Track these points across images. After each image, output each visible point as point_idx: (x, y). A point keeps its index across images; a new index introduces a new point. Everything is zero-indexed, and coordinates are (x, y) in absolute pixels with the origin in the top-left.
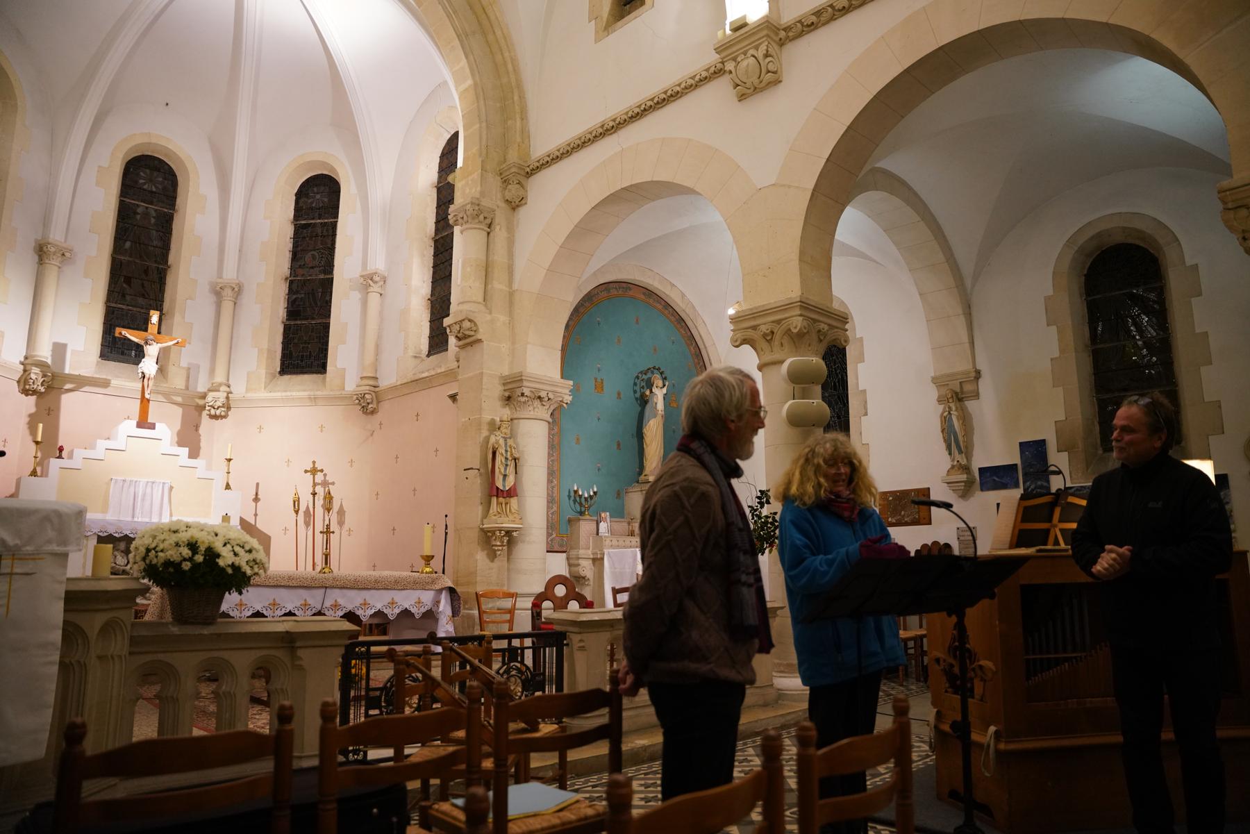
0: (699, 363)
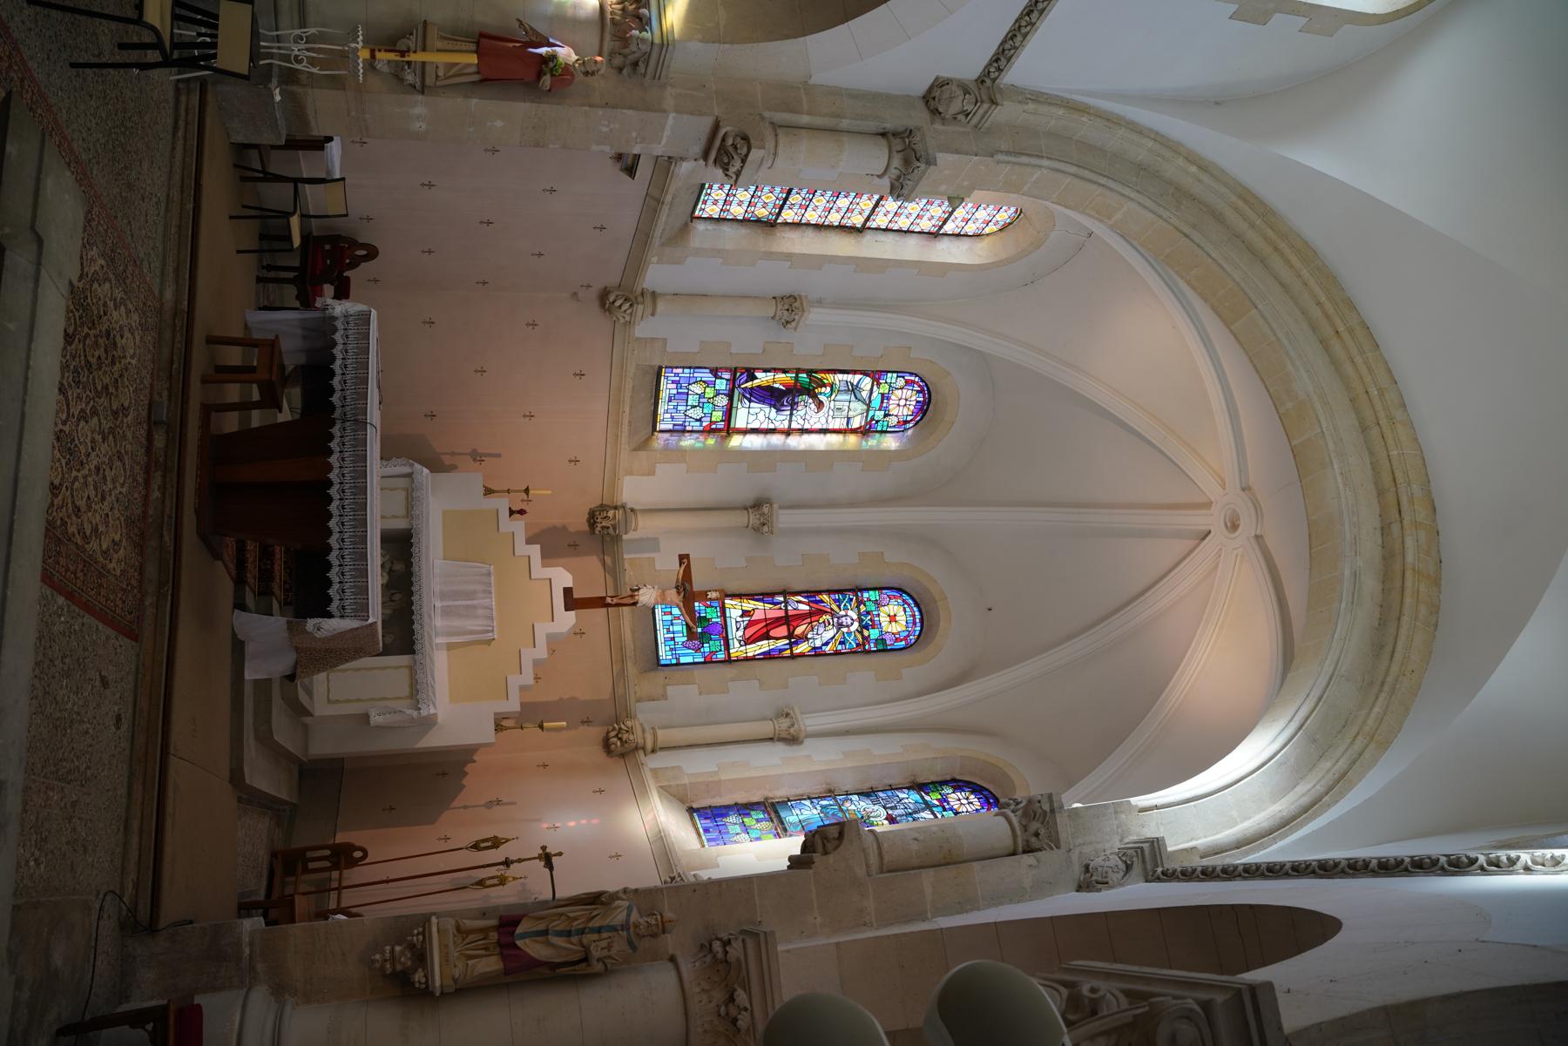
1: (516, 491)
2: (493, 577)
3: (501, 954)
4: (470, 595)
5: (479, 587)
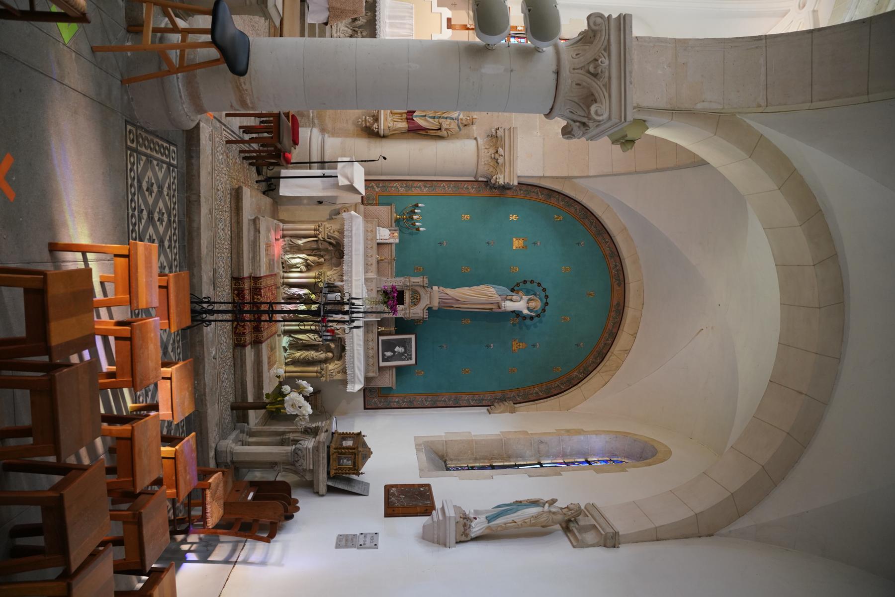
0: (562, 384)
3: (407, 122)
4: (402, 18)
5: (407, 14)
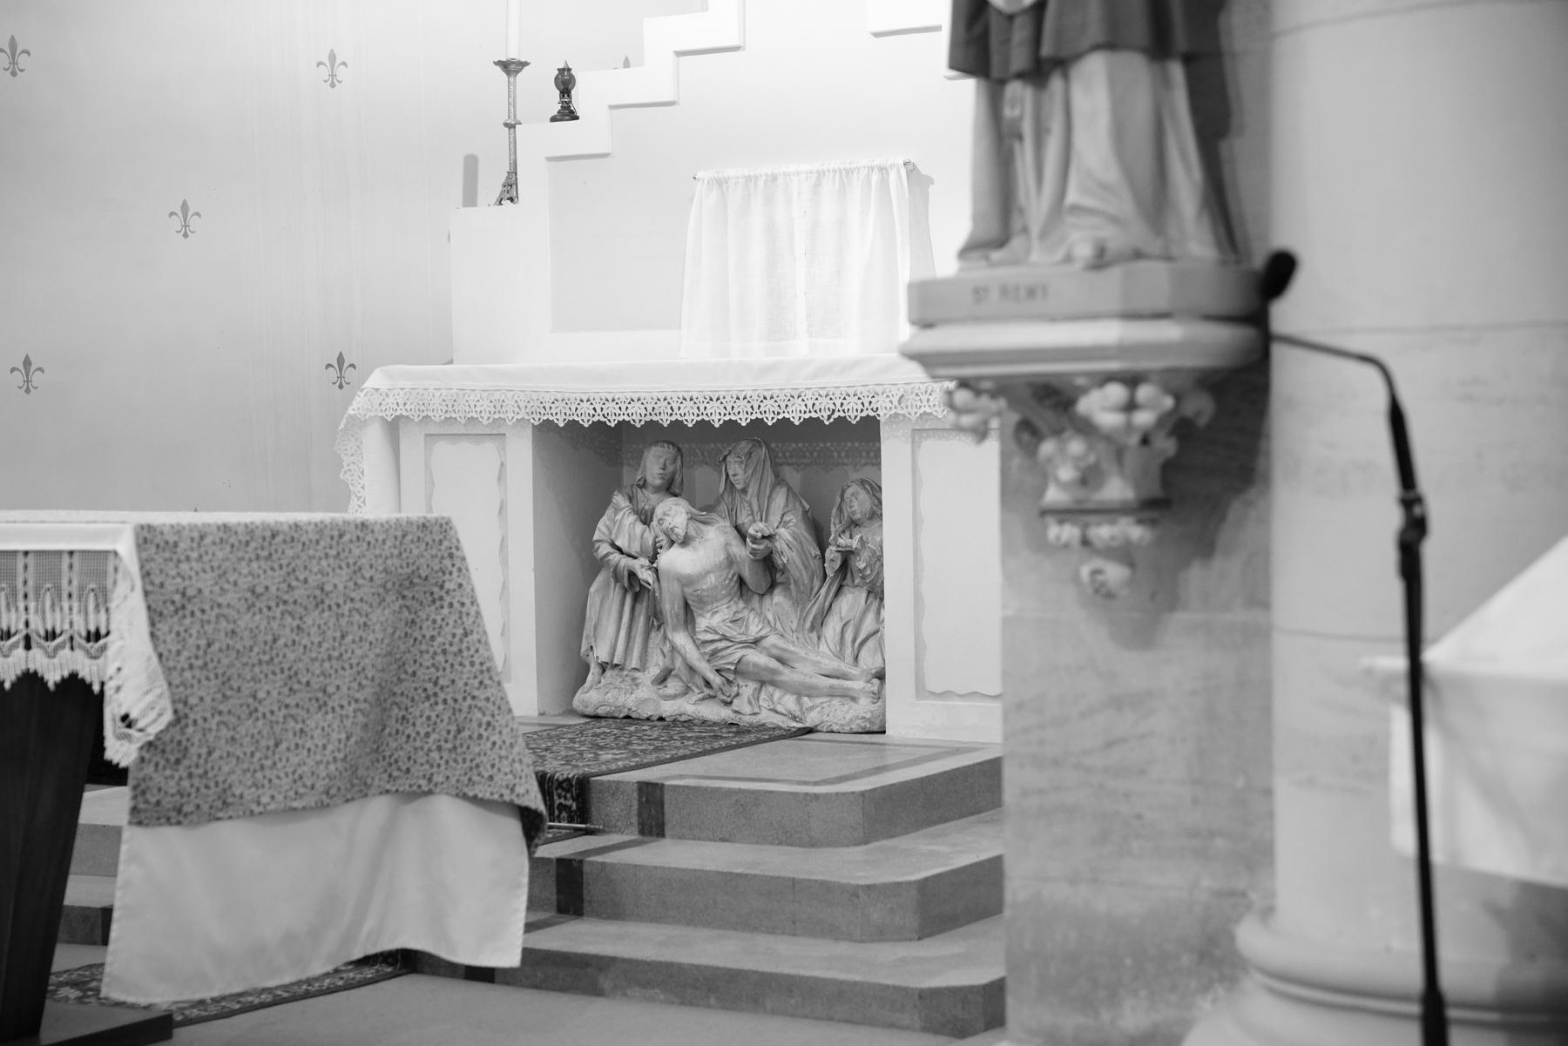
1: (512, 103)
2: (731, 172)
